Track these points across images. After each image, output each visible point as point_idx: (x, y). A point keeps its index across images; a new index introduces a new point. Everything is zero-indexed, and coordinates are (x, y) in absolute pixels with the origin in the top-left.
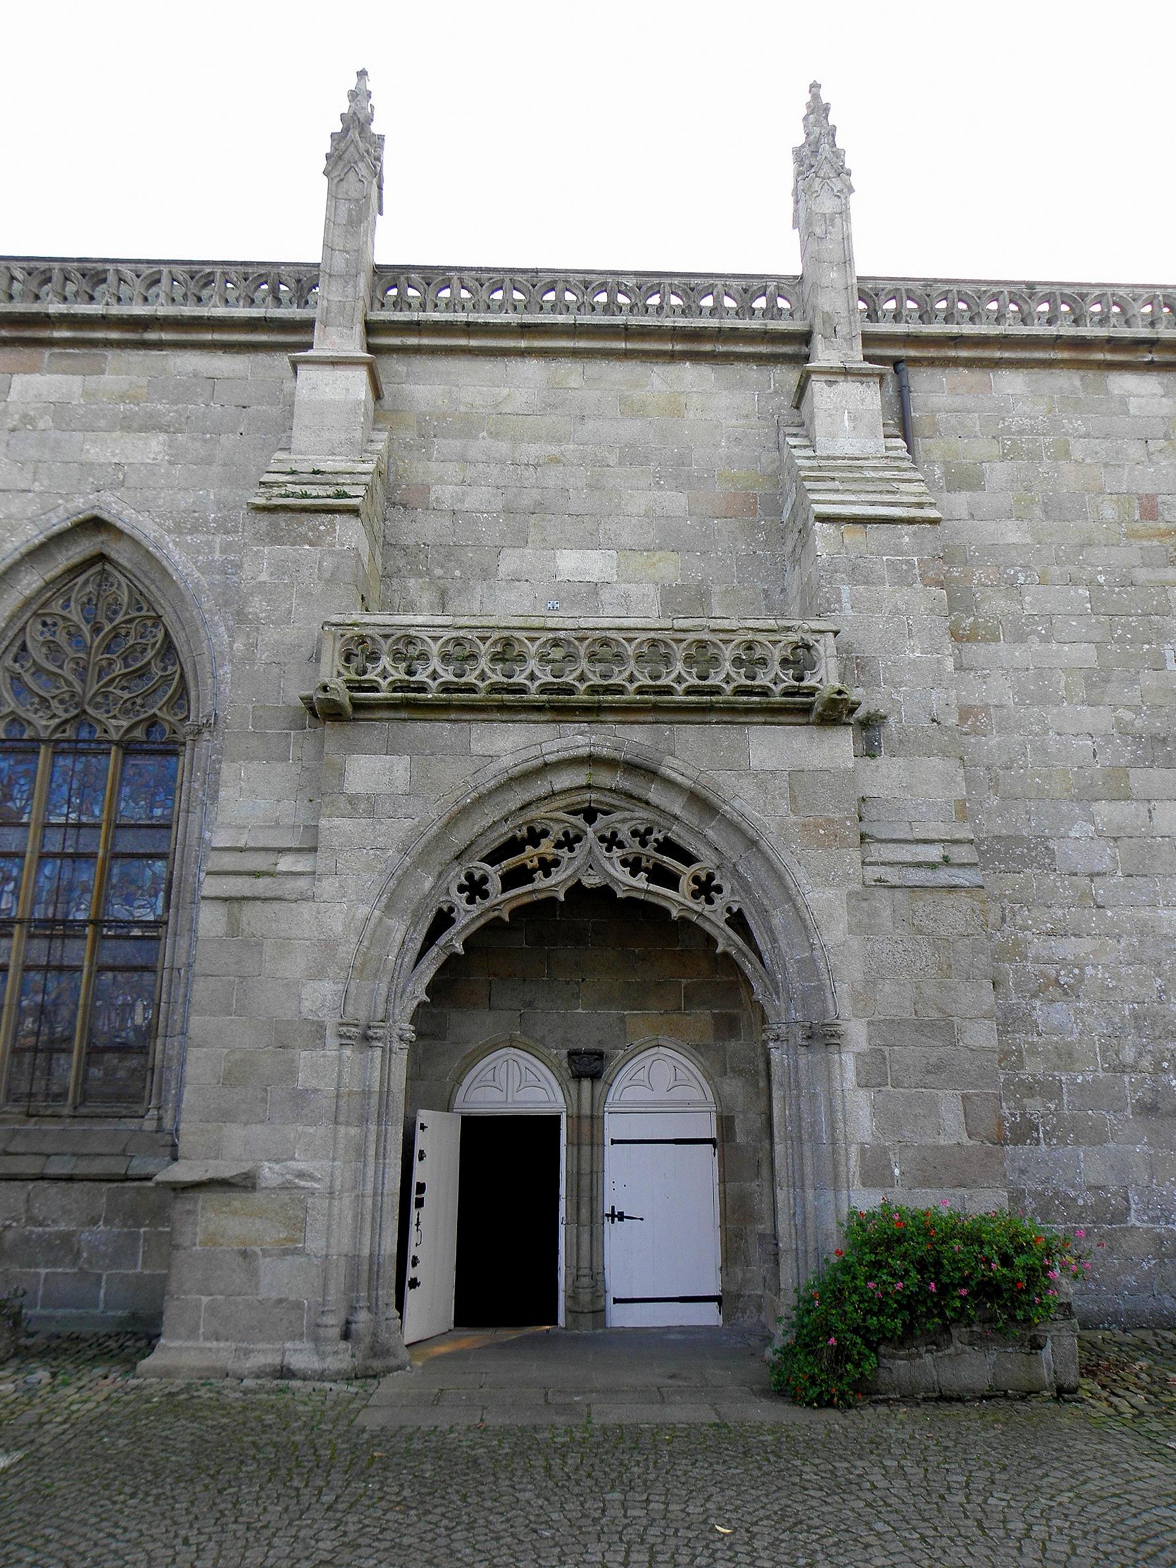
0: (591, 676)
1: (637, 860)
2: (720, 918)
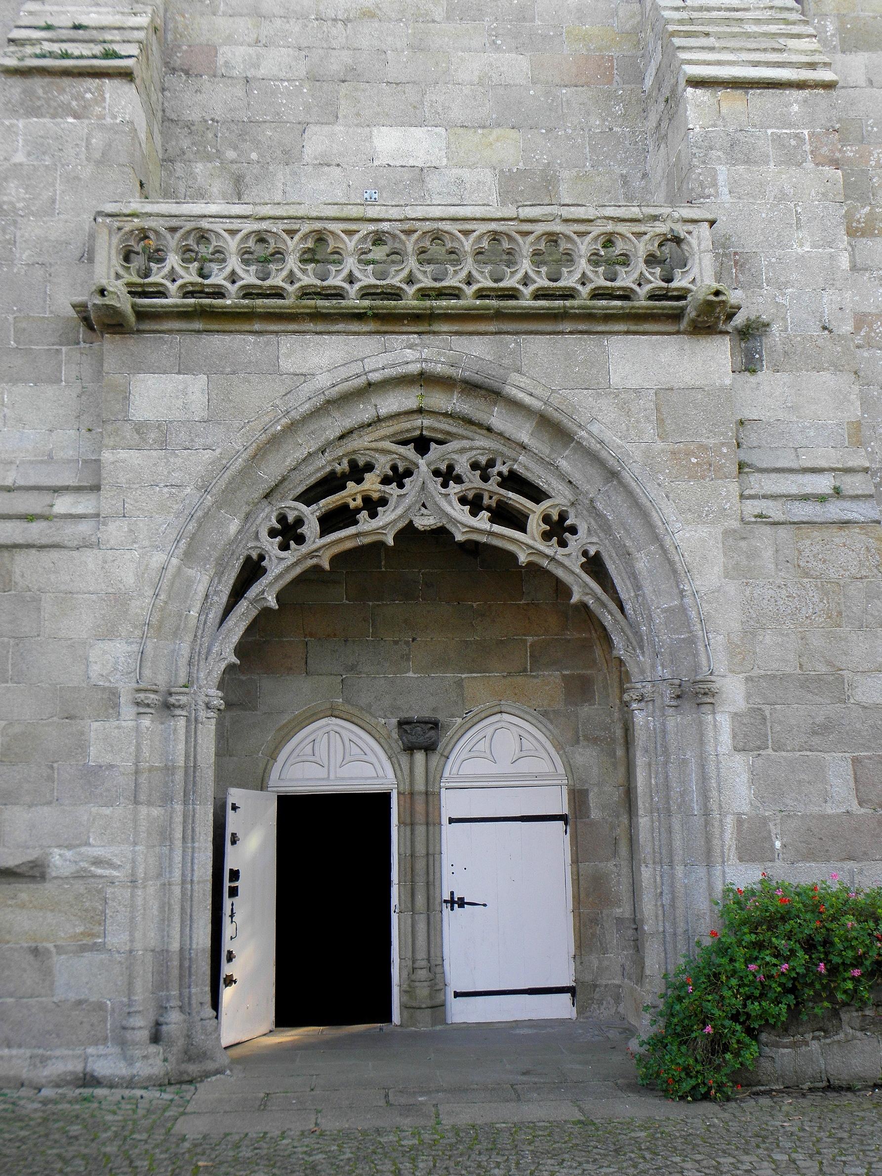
0: (420, 276)
1: (479, 497)
2: (575, 563)
